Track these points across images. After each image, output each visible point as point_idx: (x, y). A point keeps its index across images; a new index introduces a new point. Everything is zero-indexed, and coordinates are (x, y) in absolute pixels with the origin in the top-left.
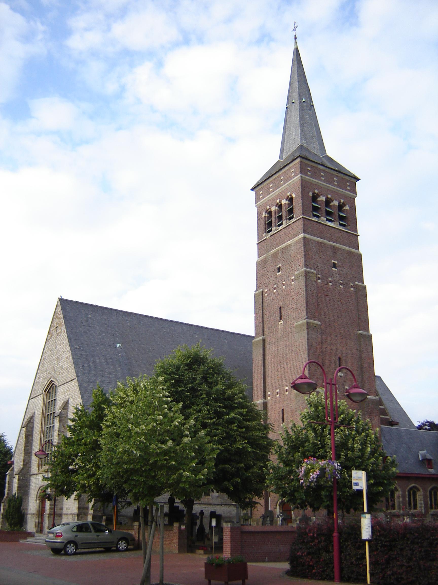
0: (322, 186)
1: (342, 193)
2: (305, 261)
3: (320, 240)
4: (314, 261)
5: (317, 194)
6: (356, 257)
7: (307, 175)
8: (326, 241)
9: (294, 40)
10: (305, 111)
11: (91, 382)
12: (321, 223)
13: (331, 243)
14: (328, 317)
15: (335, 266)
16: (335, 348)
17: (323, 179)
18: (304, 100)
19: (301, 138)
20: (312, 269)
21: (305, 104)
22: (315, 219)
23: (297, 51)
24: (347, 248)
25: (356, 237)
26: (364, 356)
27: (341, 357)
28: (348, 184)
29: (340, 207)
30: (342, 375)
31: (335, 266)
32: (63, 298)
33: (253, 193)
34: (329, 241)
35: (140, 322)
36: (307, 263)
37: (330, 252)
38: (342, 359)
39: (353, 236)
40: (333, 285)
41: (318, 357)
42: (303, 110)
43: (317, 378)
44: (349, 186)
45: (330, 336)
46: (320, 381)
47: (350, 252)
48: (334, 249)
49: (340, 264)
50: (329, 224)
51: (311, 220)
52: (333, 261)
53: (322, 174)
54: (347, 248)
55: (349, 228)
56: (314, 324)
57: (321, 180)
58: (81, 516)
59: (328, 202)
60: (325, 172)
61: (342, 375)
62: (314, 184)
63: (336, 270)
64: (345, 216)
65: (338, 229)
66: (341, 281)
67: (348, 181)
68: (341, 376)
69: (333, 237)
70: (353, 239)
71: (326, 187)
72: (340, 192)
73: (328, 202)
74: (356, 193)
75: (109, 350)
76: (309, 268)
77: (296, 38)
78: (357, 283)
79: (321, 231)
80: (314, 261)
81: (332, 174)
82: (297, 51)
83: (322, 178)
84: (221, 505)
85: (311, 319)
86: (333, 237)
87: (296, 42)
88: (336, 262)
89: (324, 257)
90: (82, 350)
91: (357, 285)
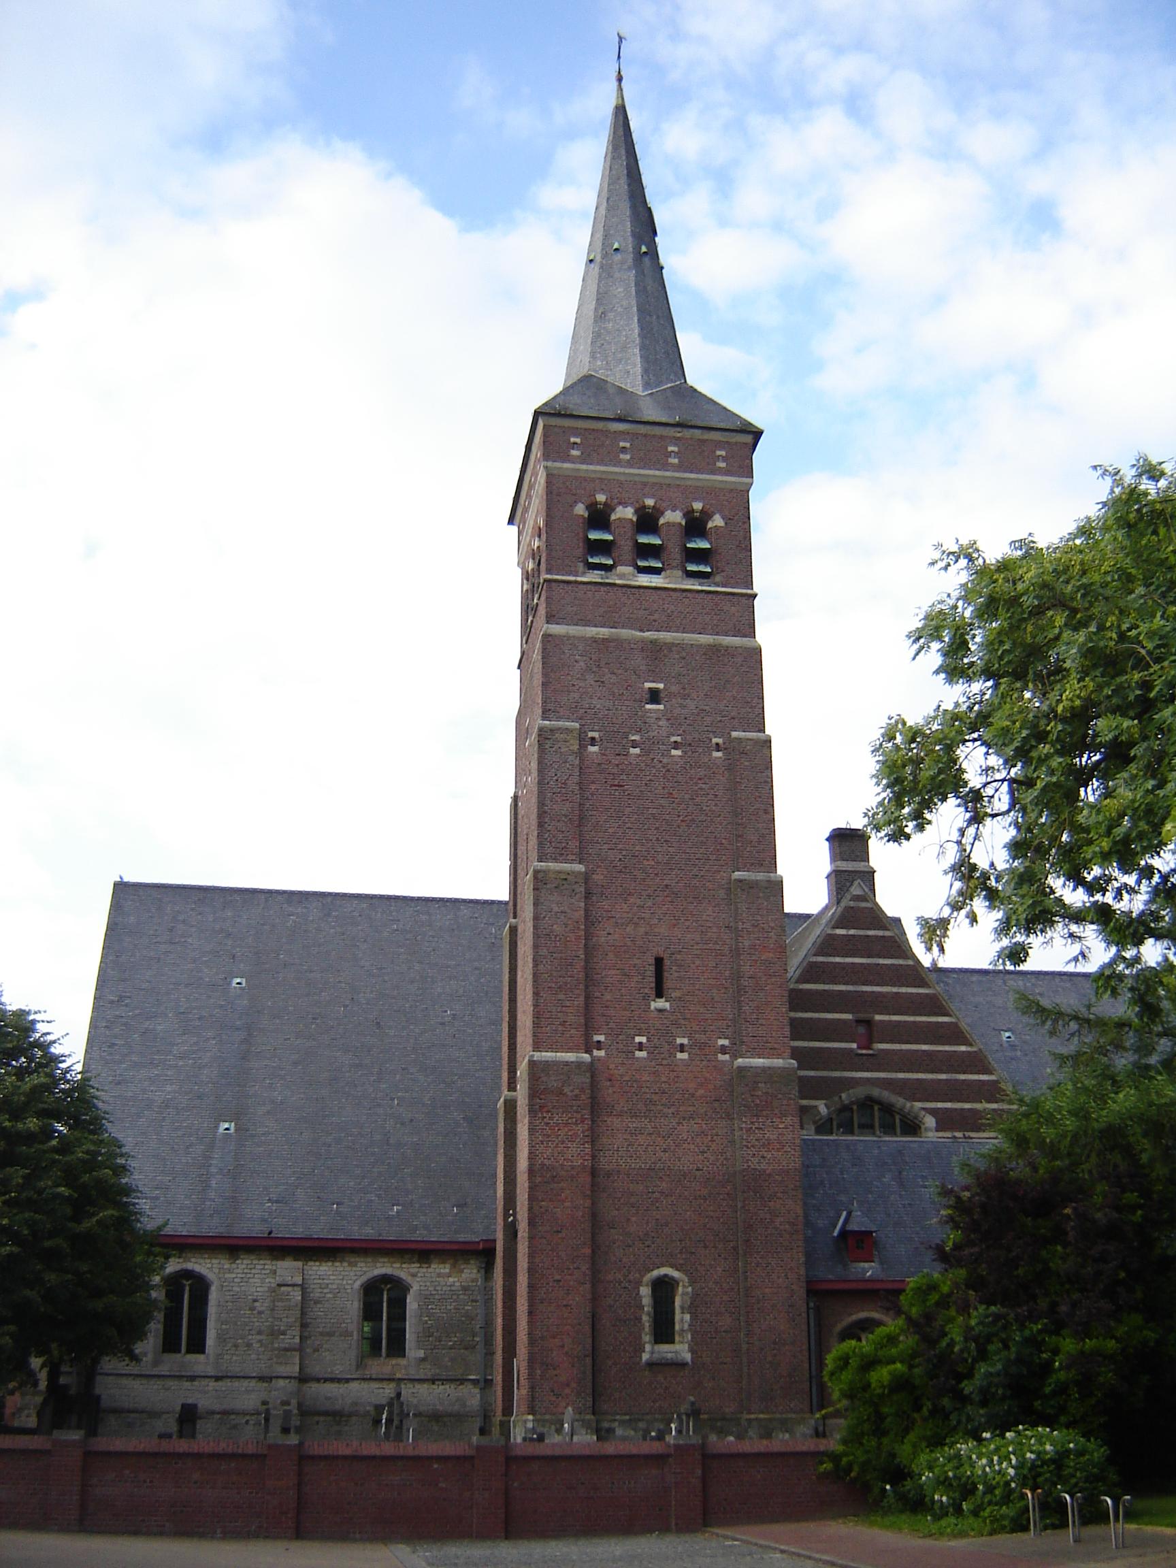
0: (622, 478)
1: (722, 486)
2: (544, 702)
3: (604, 632)
4: (576, 695)
5: (605, 504)
6: (739, 660)
7: (567, 458)
8: (625, 633)
9: (615, 84)
10: (617, 275)
11: (119, 1083)
12: (614, 584)
13: (647, 634)
14: (620, 846)
15: (654, 697)
16: (642, 930)
17: (628, 457)
18: (616, 246)
19: (593, 356)
20: (568, 719)
21: (618, 257)
22: (594, 576)
23: (621, 113)
24: (705, 639)
25: (744, 600)
26: (747, 943)
27: (666, 956)
28: (719, 453)
29: (695, 525)
30: (667, 1005)
31: (654, 697)
32: (125, 880)
33: (514, 529)
34: (641, 631)
35: (329, 915)
36: (550, 706)
37: (639, 661)
38: (667, 962)
39: (735, 599)
40: (646, 752)
41: (571, 965)
42: (610, 276)
43: (563, 1023)
44: (724, 459)
45: (626, 900)
46: (573, 1031)
47: (714, 651)
48: (655, 651)
49: (674, 689)
50: (644, 580)
51: (576, 582)
52: (648, 685)
53: (622, 444)
54: (705, 639)
55: (718, 578)
56: (560, 872)
57: (619, 463)
58: (26, 1412)
59: (647, 521)
60: (633, 436)
61: (667, 1005)
62: (593, 480)
63: (661, 707)
64: (714, 548)
65: (675, 590)
66: (673, 739)
67: (719, 445)
68: (660, 1011)
69: (656, 616)
70: (740, 612)
71: (637, 479)
72: (689, 483)
73: (647, 521)
74: (750, 474)
75: (204, 997)
76: (559, 719)
77: (620, 79)
78: (734, 734)
79: (618, 605)
80: (576, 695)
81: (661, 437)
82: (621, 113)
83: (622, 456)
84: (433, 1381)
85: (555, 860)
86: (656, 616)
87: (620, 89)
88: (661, 686)
89: (614, 679)
90: (126, 1005)
91: (739, 740)
